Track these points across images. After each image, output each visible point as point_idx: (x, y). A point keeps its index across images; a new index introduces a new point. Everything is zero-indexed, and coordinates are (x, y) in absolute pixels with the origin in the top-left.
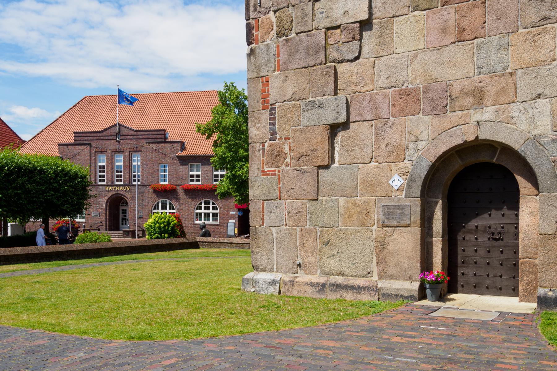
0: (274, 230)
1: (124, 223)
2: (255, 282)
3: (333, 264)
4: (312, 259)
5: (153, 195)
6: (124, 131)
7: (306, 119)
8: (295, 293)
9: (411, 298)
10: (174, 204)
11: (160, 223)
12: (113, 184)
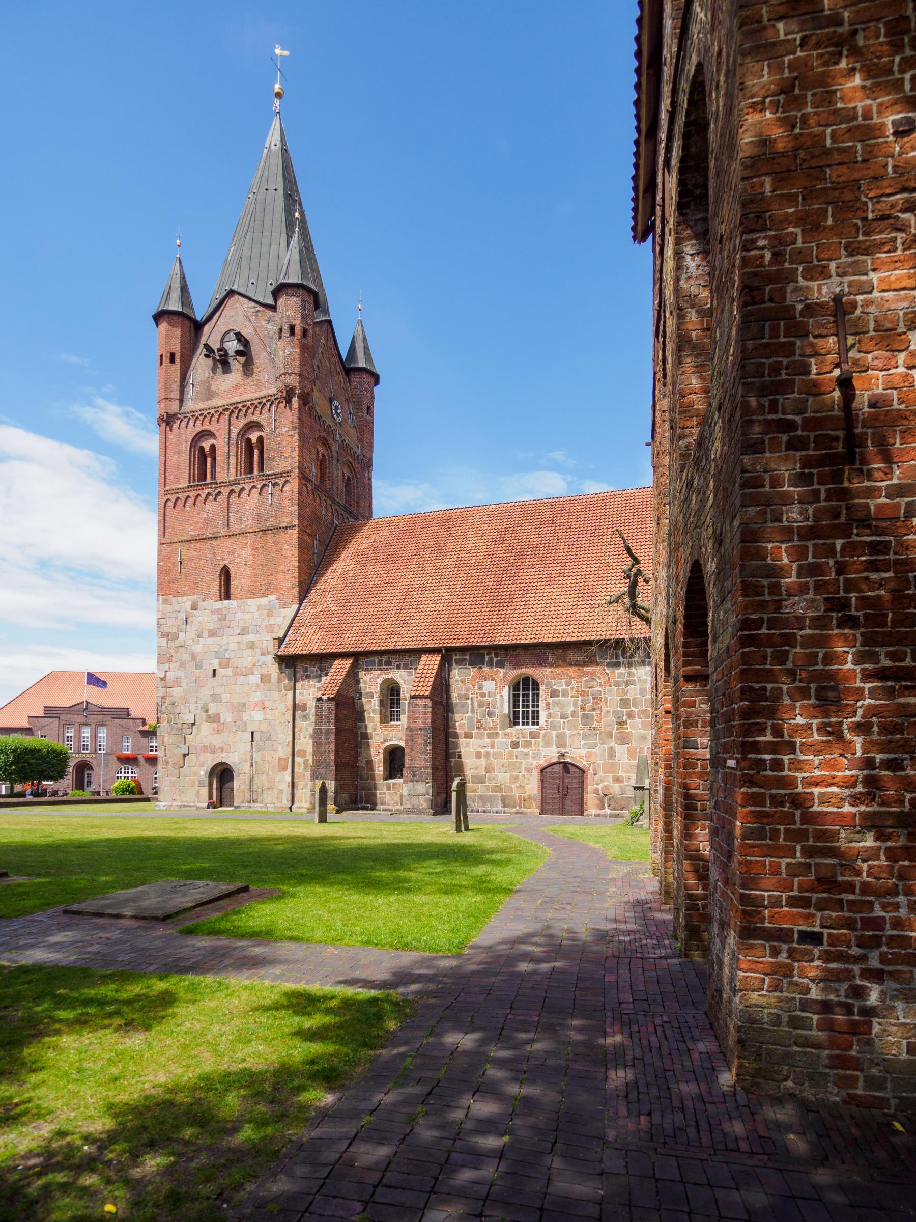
1: (89, 785)
3: (184, 799)
6: (91, 708)
7: (177, 751)
10: (135, 769)
12: (79, 753)
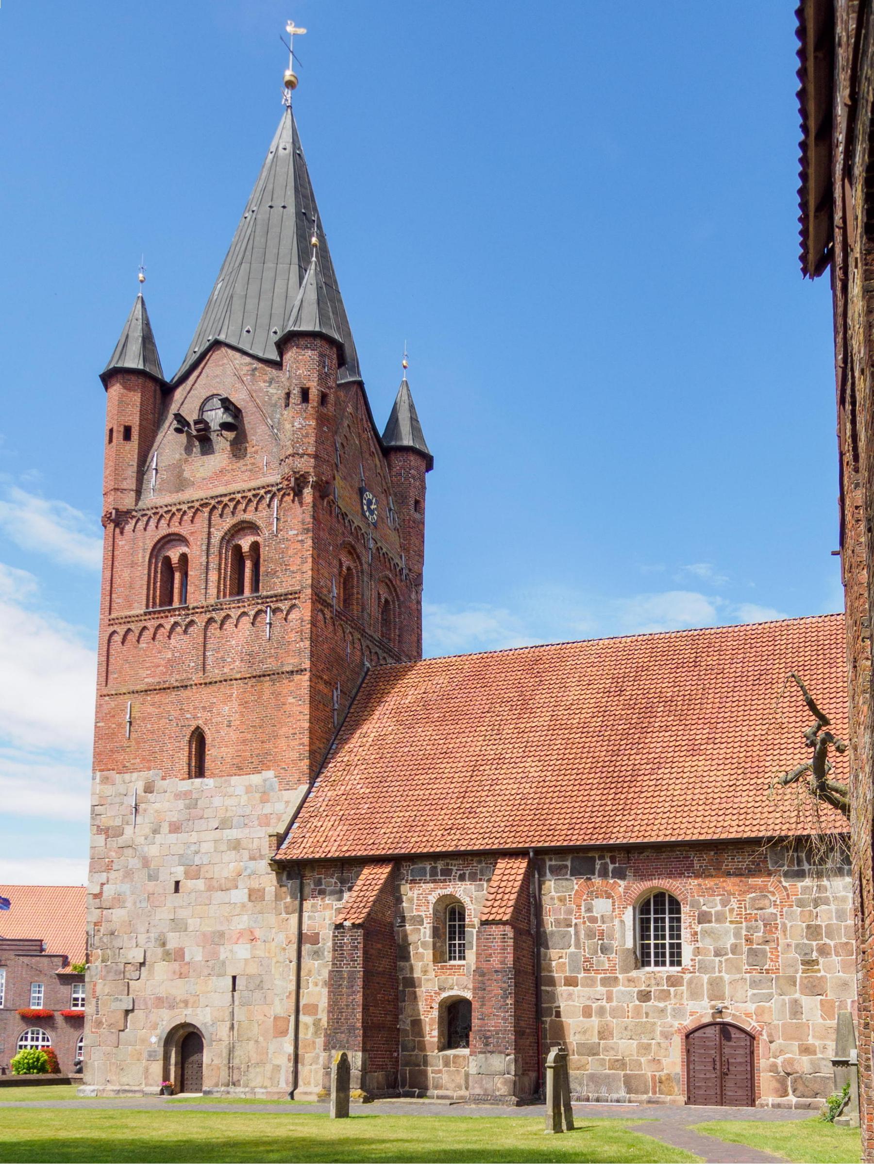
0: (96, 1063)
2: (84, 1091)
3: (124, 1080)
4: (114, 1078)
5: (21, 1022)
7: (115, 1005)
8: (104, 1095)
10: (49, 1034)
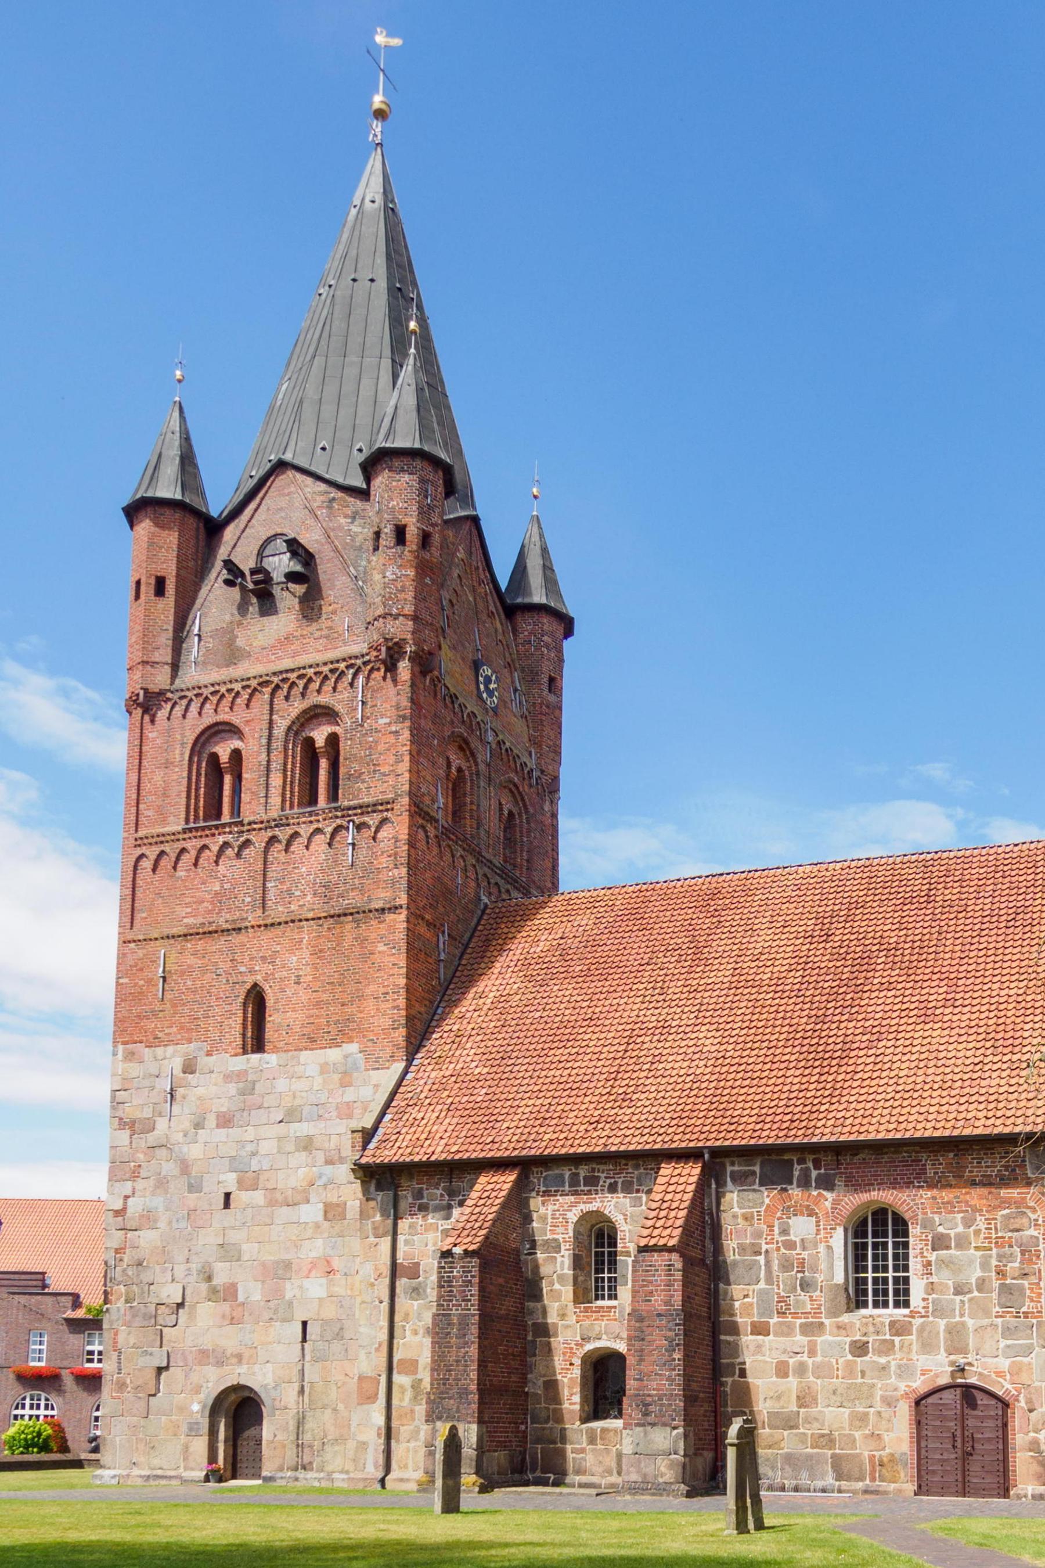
0: (118, 1439)
2: (101, 1477)
3: (156, 1462)
4: (142, 1459)
8: (129, 1483)
9: (200, 1481)
11: (27, 1434)
